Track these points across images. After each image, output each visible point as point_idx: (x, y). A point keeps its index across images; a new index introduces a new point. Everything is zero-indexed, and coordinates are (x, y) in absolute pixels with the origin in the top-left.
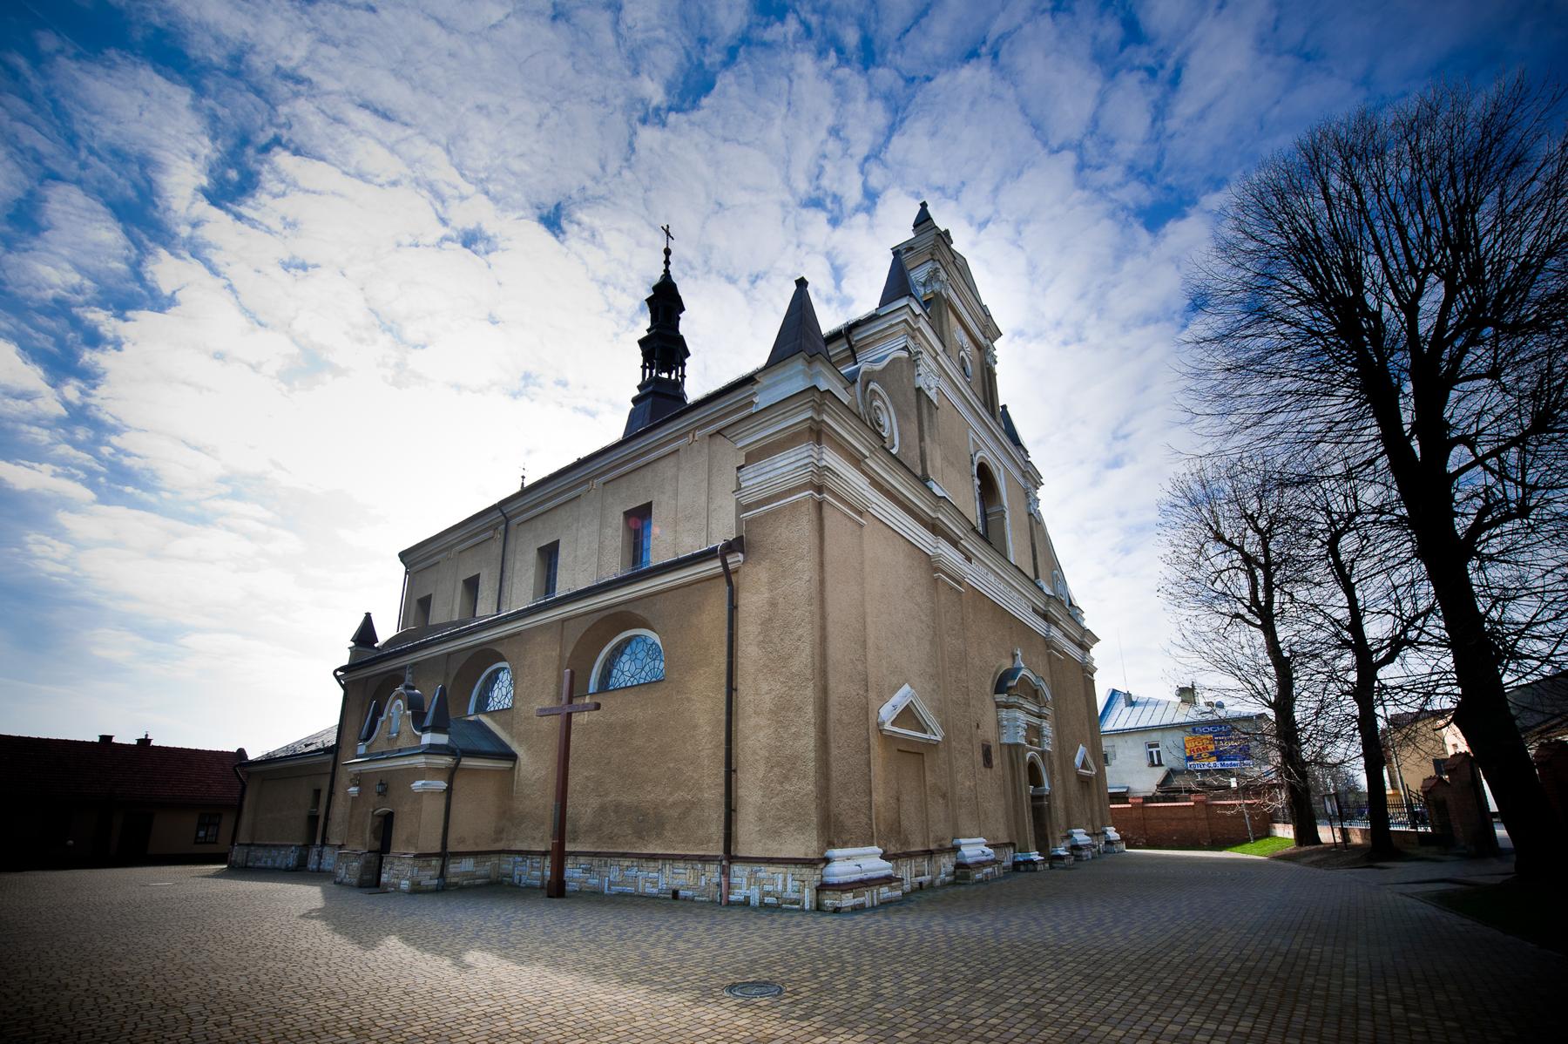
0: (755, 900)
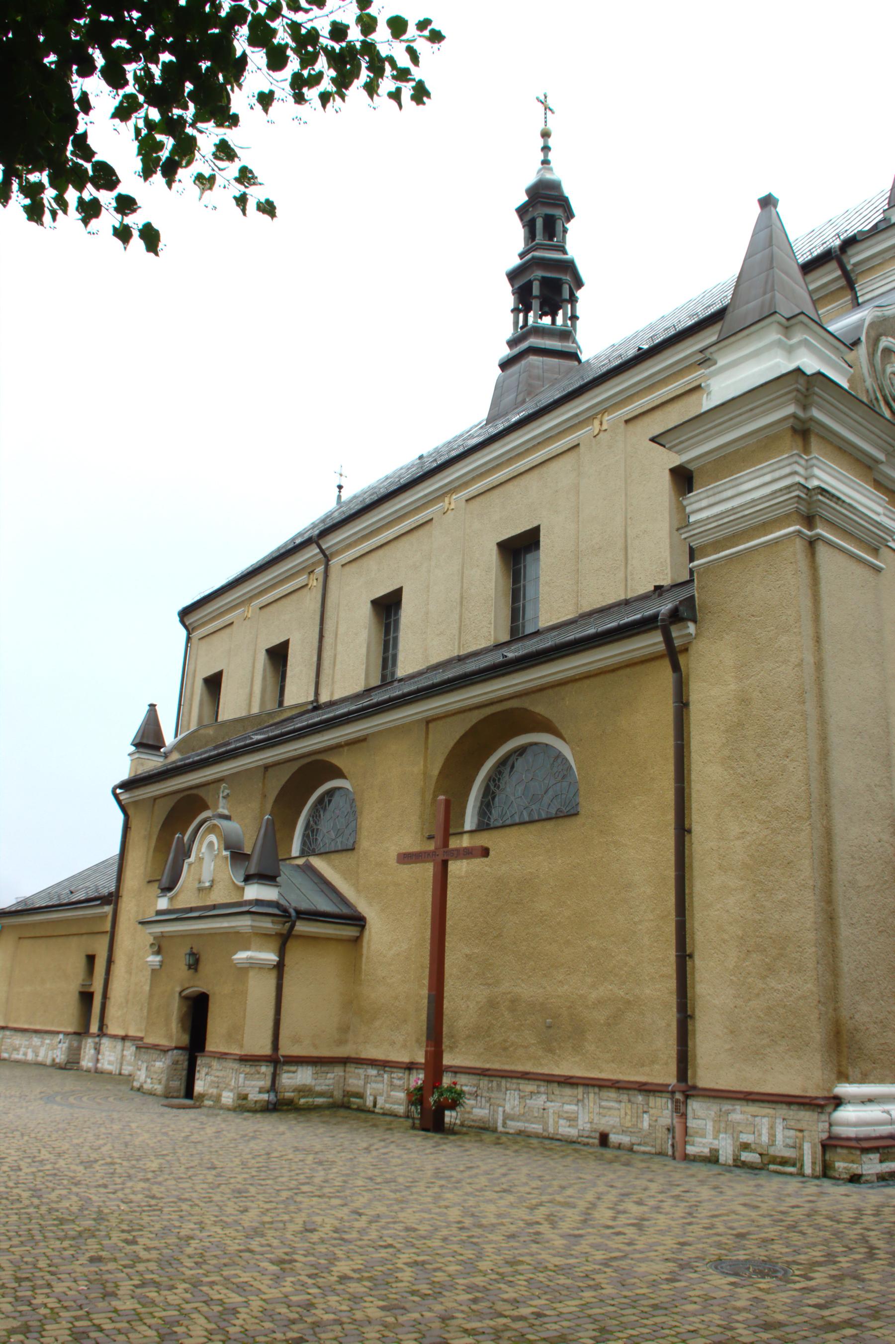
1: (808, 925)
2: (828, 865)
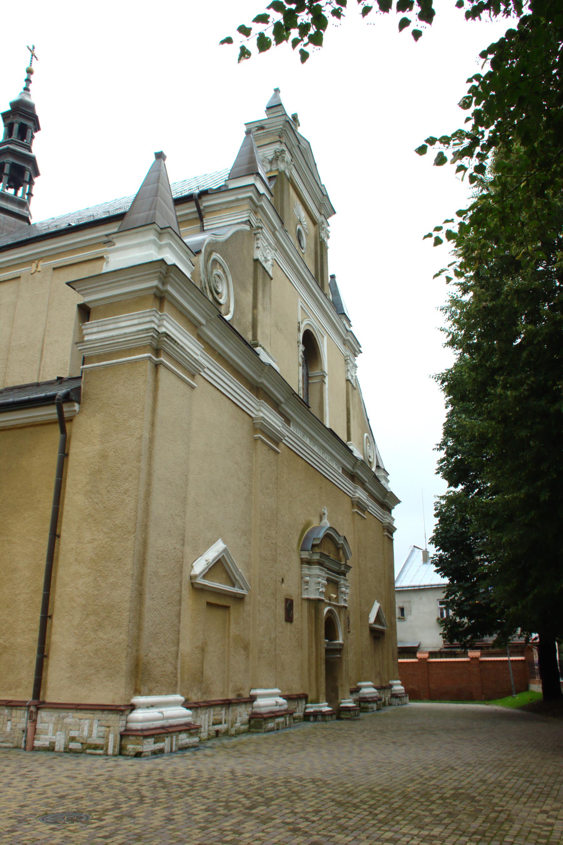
0: (60, 742)
1: (127, 598)
2: (142, 562)
